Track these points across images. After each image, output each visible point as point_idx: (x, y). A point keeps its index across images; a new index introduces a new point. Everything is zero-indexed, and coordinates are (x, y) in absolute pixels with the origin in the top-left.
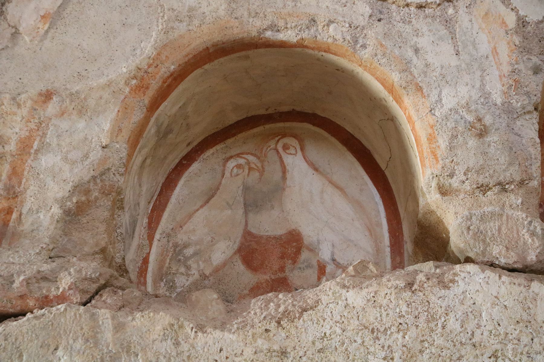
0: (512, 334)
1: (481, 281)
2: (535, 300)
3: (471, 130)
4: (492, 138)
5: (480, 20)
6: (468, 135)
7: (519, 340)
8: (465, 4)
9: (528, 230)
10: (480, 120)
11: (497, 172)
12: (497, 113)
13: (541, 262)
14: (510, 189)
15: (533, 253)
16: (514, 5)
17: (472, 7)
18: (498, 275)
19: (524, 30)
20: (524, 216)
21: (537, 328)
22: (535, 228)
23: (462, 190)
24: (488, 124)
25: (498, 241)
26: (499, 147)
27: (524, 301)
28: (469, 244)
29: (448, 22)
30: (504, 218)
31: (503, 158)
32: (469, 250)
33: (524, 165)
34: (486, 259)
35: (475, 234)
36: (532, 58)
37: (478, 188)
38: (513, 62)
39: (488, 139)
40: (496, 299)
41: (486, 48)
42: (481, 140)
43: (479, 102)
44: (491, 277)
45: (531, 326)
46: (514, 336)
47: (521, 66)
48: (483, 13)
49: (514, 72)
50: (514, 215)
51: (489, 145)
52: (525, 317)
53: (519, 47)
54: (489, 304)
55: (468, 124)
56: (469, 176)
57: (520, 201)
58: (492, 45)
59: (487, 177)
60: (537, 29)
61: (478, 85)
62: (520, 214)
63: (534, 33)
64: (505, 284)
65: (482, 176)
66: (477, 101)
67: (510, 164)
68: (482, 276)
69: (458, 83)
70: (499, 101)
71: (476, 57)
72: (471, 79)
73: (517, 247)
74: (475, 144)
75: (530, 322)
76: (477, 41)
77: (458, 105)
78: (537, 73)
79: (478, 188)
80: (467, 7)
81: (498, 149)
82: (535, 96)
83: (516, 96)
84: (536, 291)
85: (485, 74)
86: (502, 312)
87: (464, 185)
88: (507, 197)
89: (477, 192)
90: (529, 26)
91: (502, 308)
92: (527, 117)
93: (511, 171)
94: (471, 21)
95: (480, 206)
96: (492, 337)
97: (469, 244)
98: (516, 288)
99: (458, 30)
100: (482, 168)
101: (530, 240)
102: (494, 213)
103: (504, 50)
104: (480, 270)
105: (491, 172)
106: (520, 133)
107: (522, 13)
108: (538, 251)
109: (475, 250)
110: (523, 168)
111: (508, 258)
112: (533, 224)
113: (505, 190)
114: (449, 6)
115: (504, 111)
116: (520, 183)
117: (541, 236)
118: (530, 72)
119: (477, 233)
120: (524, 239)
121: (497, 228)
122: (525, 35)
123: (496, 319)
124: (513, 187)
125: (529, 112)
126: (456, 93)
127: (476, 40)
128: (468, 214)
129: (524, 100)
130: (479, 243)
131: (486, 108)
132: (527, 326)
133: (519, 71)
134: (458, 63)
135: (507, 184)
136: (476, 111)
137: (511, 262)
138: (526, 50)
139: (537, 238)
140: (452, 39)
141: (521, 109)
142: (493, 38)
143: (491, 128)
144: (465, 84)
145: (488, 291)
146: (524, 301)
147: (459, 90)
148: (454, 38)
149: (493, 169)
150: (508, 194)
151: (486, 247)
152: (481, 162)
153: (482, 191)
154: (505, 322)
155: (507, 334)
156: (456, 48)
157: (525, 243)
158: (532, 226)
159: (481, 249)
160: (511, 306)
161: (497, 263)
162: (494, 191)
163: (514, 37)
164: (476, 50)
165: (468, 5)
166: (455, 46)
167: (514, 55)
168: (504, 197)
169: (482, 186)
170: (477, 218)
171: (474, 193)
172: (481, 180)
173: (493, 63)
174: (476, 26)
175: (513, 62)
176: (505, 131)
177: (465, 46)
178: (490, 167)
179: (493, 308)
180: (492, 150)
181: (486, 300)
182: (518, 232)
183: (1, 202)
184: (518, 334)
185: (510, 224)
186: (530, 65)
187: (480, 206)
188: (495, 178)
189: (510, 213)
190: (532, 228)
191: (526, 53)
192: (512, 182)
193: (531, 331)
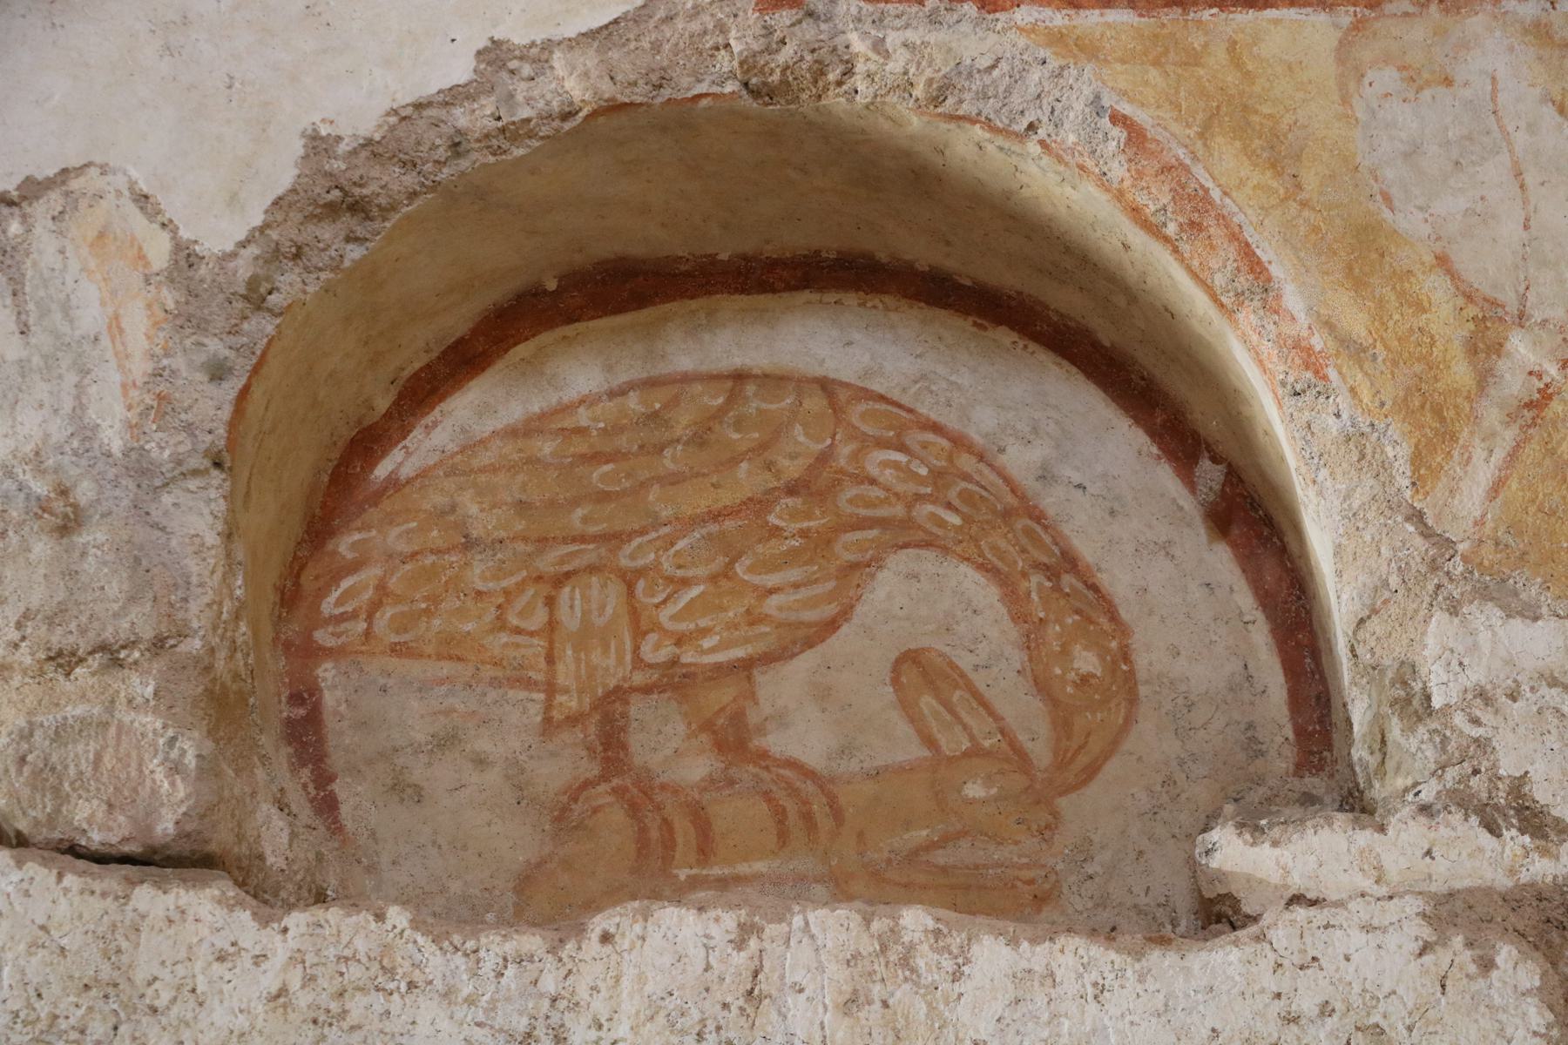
0: (67, 1017)
1: (10, 889)
2: (137, 930)
3: (41, 517)
4: (93, 535)
5: (85, 251)
6: (32, 529)
7: (82, 1032)
8: (51, 212)
9: (166, 759)
10: (64, 492)
11: (98, 619)
12: (110, 476)
13: (188, 835)
14: (130, 660)
15: (170, 816)
16: (168, 216)
17: (67, 217)
18: (55, 872)
19: (190, 274)
20: (159, 724)
21: (130, 998)
22: (183, 752)
23: (16, 666)
24: (83, 501)
25: (92, 788)
26: (107, 558)
27: (109, 936)
28: (18, 799)
29: (7, 255)
30: (113, 731)
31: (114, 584)
32: (18, 813)
33: (166, 600)
34: (57, 835)
35: (36, 773)
36: (206, 341)
37: (50, 658)
38: (158, 351)
39: (81, 539)
40: (41, 933)
41: (95, 318)
42: (65, 541)
43: (67, 449)
44: (38, 879)
45: (118, 996)
46: (72, 1021)
47: (179, 362)
48: (92, 234)
49: (161, 376)
50: (136, 724)
51: (84, 554)
52: (106, 972)
53: (176, 316)
54: (22, 947)
55: (34, 503)
56: (29, 630)
57: (150, 690)
58: (110, 310)
59: (71, 632)
60: (222, 272)
61: (68, 404)
62: (150, 722)
63: (214, 281)
64: (69, 895)
65: (59, 631)
66: (61, 447)
67: (132, 599)
68: (16, 876)
69: (20, 404)
70: (116, 447)
71: (68, 340)
72: (51, 393)
73: (134, 801)
74: (49, 552)
75: (116, 985)
76: (74, 302)
77: (15, 457)
78: (221, 379)
79: (50, 658)
80: (54, 218)
81: (105, 563)
82: (210, 433)
83: (160, 434)
84: (142, 908)
85: (86, 381)
86: (52, 964)
87: (18, 654)
88: (123, 681)
89: (49, 667)
90: (203, 266)
91: (52, 953)
92: (193, 484)
93: (133, 616)
94: (62, 252)
95: (57, 705)
96: (19, 1027)
97: (18, 799)
98: (96, 904)
99: (29, 274)
100: (62, 610)
101: (166, 785)
102: (89, 720)
103: (137, 323)
104: (12, 863)
105: (84, 619)
106: (164, 522)
107: (185, 234)
108: (183, 809)
109: (34, 814)
110: (164, 609)
111: (110, 829)
112: (178, 745)
113: (118, 663)
114: (12, 214)
115: (127, 468)
116: (154, 644)
117: (193, 774)
118: (201, 377)
119: (42, 770)
120: (154, 781)
121: (91, 756)
122: (192, 287)
123: (35, 981)
124: (137, 654)
125: (196, 473)
126: (13, 427)
127: (72, 297)
128: (24, 724)
129: (180, 443)
130: (44, 796)
131: (84, 462)
132: (106, 997)
133: (173, 372)
134: (24, 354)
135: (123, 647)
136: (56, 471)
137: (114, 840)
138: (194, 322)
139: (183, 779)
140: (15, 295)
141: (172, 465)
142: (114, 293)
143: (92, 511)
144: (36, 406)
145: (26, 913)
146: (109, 936)
147: (19, 419)
148: (20, 294)
149: (88, 613)
150: (126, 671)
151: (61, 805)
152: (61, 595)
153: (60, 665)
154: (56, 989)
155: (56, 1017)
156: (23, 317)
157: (154, 792)
158: (176, 750)
159: (48, 810)
160: (75, 948)
161: (83, 843)
162: (89, 667)
163: (165, 291)
164: (71, 321)
165: (56, 213)
166: (19, 313)
167: (161, 335)
168: (114, 681)
169: (60, 654)
170: (45, 733)
171: (42, 673)
172: (58, 639)
173: (109, 355)
174: (74, 265)
175: (158, 351)
176: (127, 517)
177: (44, 313)
178: (82, 607)
179: (31, 954)
180: (90, 564)
181: (17, 938)
182: (140, 765)
183: (1567, 745)
184: (83, 1016)
185: (124, 745)
186: (201, 358)
187: (57, 705)
188: (92, 634)
189: (127, 719)
190: (174, 754)
191: (191, 331)
192: (133, 642)
193: (115, 1006)
